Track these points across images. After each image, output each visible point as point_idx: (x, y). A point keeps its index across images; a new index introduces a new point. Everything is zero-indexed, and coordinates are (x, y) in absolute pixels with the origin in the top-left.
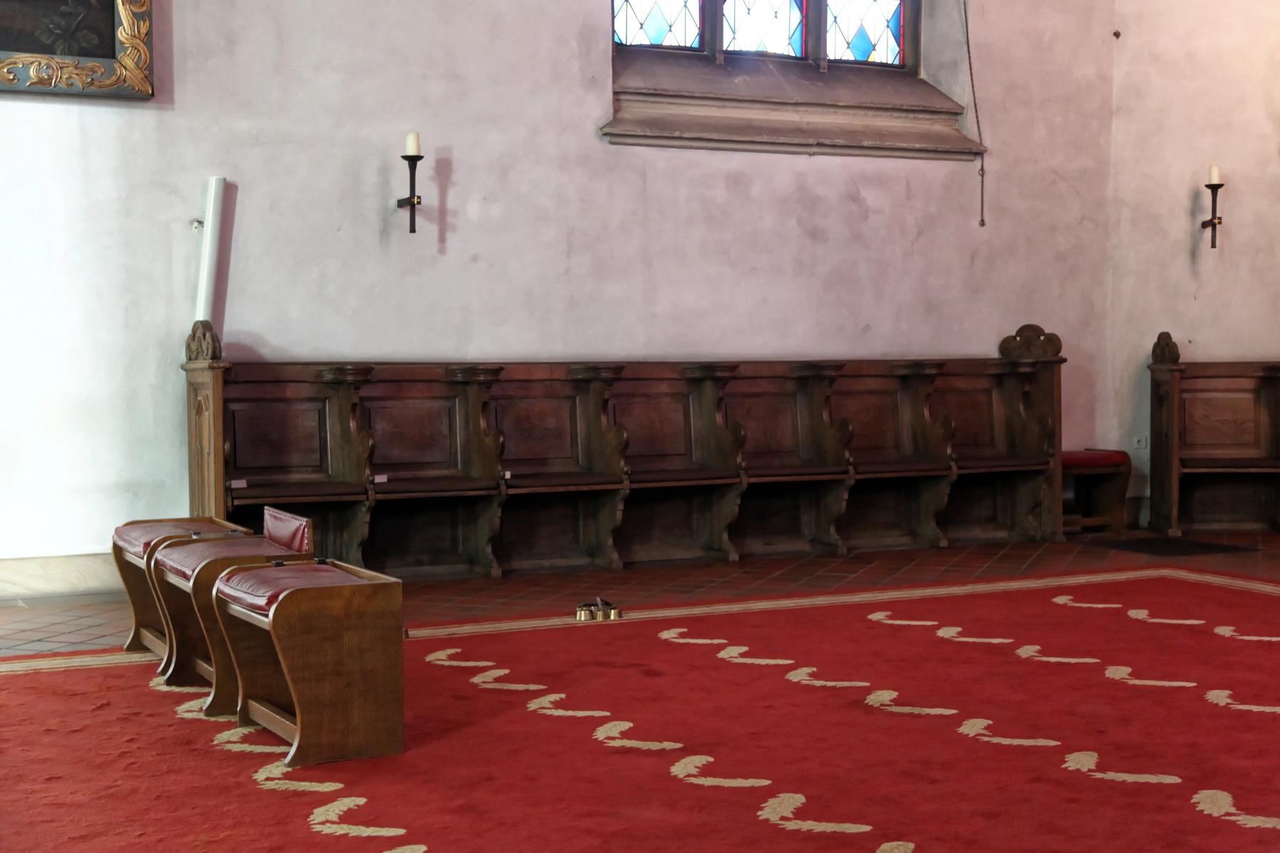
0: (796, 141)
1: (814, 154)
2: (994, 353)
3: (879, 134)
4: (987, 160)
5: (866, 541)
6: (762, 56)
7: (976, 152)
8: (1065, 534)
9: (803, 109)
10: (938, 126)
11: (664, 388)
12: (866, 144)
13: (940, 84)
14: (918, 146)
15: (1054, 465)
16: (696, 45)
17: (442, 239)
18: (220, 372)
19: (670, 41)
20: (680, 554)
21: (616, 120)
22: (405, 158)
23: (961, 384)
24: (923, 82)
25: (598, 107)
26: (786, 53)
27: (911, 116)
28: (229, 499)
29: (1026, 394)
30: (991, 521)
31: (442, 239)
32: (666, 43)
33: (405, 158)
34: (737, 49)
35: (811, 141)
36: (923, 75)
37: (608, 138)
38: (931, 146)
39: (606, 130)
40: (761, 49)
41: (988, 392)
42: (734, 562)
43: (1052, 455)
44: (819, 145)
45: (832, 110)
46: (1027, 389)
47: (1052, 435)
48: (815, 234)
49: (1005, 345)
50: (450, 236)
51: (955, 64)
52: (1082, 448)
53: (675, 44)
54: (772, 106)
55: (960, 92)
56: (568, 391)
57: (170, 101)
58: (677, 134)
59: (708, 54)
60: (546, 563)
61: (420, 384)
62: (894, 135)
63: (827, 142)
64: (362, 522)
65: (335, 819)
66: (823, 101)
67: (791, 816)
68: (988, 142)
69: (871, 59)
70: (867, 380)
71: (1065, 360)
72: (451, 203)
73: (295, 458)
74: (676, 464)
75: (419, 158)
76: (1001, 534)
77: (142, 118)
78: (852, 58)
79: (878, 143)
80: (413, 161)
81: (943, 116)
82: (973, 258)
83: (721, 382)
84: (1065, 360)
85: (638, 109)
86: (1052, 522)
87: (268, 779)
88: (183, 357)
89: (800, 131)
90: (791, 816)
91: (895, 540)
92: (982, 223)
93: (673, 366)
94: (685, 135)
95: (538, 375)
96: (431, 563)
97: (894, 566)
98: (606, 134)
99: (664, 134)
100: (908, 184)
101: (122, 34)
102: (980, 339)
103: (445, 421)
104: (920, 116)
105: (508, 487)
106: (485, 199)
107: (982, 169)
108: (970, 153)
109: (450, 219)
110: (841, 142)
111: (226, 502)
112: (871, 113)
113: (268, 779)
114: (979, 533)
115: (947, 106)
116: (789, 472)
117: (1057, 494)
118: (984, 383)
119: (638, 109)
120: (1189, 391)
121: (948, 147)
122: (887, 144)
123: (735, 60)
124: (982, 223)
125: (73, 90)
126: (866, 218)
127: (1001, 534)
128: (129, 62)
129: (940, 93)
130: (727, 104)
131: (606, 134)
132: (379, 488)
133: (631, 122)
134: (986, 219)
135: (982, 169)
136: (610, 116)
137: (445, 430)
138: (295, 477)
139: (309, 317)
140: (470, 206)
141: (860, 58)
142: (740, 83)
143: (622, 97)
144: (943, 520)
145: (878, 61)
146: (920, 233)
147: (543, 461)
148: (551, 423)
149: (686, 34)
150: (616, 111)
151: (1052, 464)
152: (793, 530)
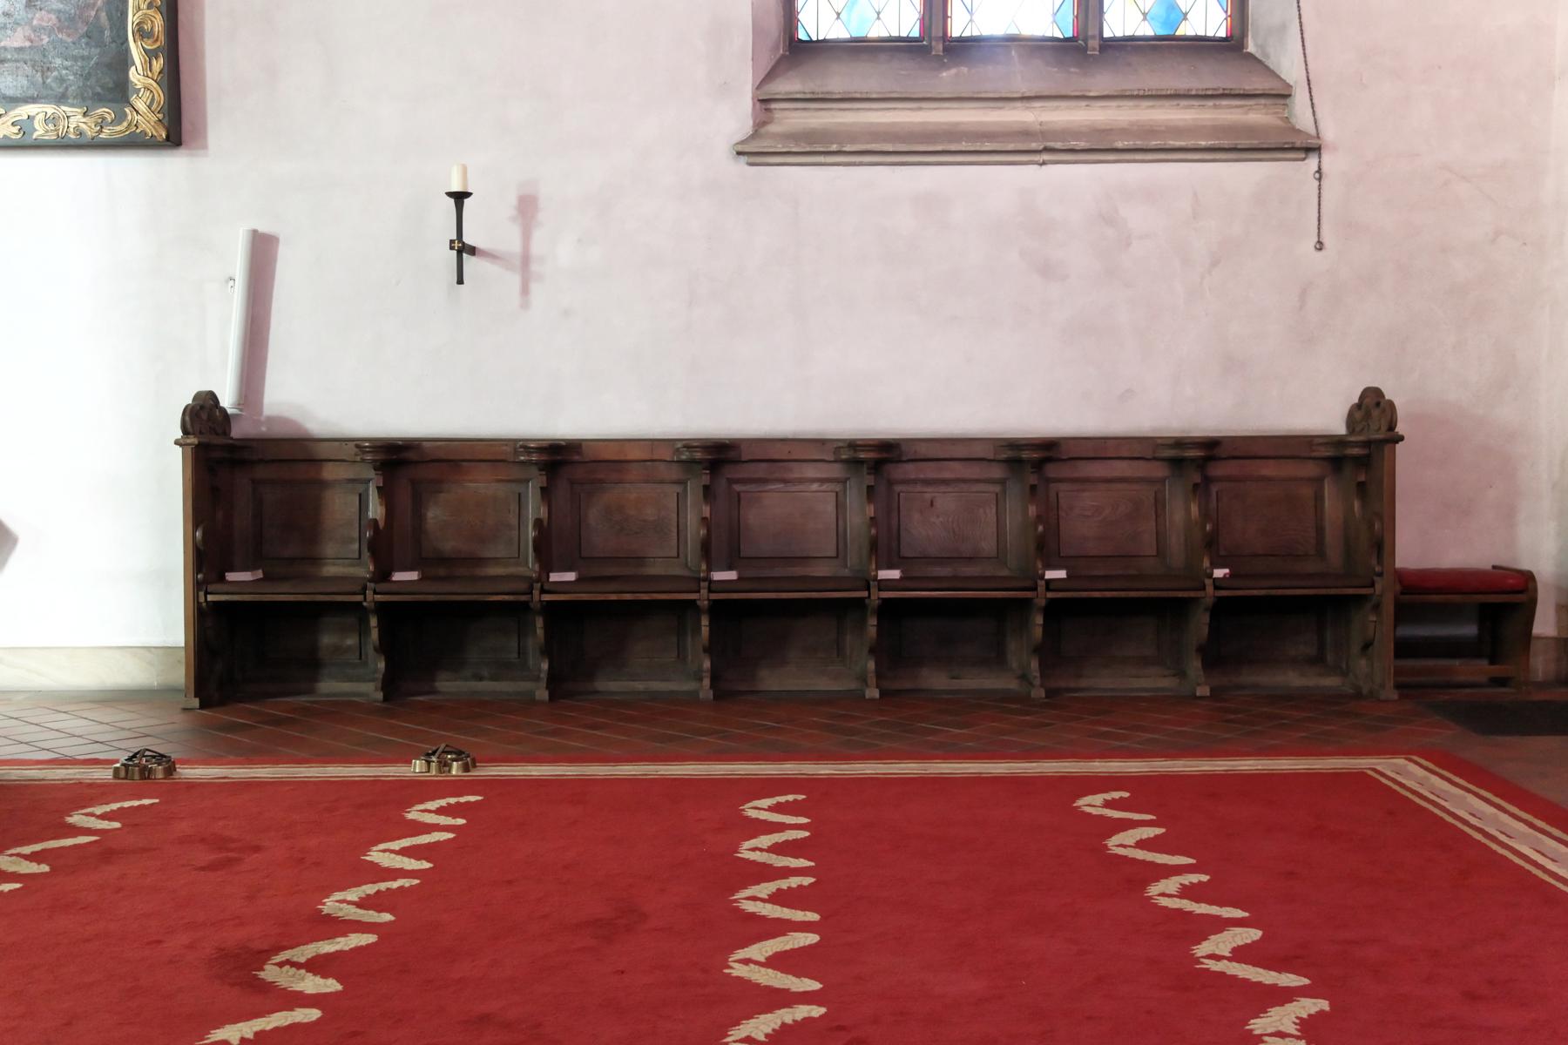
0: (1011, 147)
1: (1044, 163)
2: (1340, 428)
3: (1150, 131)
4: (1326, 157)
5: (1103, 681)
6: (1012, 41)
7: (1312, 149)
8: (1398, 686)
9: (1037, 104)
10: (1257, 116)
11: (810, 471)
12: (1119, 145)
13: (1267, 56)
14: (1203, 143)
15: (1385, 590)
16: (916, 33)
17: (525, 290)
18: (189, 449)
19: (876, 31)
20: (823, 684)
21: (755, 135)
22: (450, 194)
23: (1269, 469)
24: (1251, 56)
25: (736, 117)
26: (1049, 34)
27: (1210, 103)
28: (202, 594)
29: (1361, 485)
30: (1317, 661)
31: (525, 290)
32: (873, 34)
33: (450, 194)
34: (976, 33)
35: (1034, 146)
36: (1251, 48)
37: (744, 159)
38: (1225, 143)
39: (740, 148)
40: (1013, 31)
41: (1319, 481)
42: (872, 700)
43: (1380, 575)
44: (1047, 150)
45: (1083, 103)
46: (1362, 478)
47: (1382, 544)
48: (1048, 270)
49: (1351, 420)
50: (535, 287)
51: (1283, 28)
52: (1489, 567)
53: (885, 34)
54: (992, 104)
55: (1289, 67)
56: (675, 473)
57: (205, 147)
58: (834, 147)
59: (935, 47)
60: (640, 686)
61: (483, 465)
62: (1177, 131)
63: (1058, 145)
64: (1200, 625)
65: (762, 959)
66: (1063, 93)
67: (1292, 1029)
68: (1329, 134)
69: (1179, 32)
70: (752, 466)
71: (1402, 438)
72: (537, 248)
73: (330, 549)
74: (821, 570)
75: (468, 195)
76: (1331, 682)
77: (172, 164)
78: (1150, 32)
79: (1139, 143)
80: (460, 197)
81: (1263, 101)
82: (1303, 294)
83: (877, 467)
84: (1402, 438)
85: (793, 120)
86: (1375, 670)
87: (1163, 895)
88: (179, 434)
89: (1026, 133)
90: (1292, 1029)
91: (1154, 681)
92: (1320, 246)
93: (821, 443)
94: (847, 149)
95: (634, 454)
96: (494, 678)
97: (1115, 722)
98: (739, 153)
99: (818, 149)
100: (1195, 194)
101: (136, 76)
102: (1323, 412)
103: (514, 507)
104: (1225, 102)
105: (1048, 589)
106: (579, 240)
107: (1319, 171)
108: (1293, 149)
109: (534, 267)
110: (1082, 145)
111: (196, 597)
112: (1114, 103)
113: (1163, 895)
114: (1293, 679)
115: (1258, 84)
116: (945, 585)
117: (1379, 626)
118: (1311, 470)
119: (793, 120)
120: (738, 481)
121: (1255, 143)
122: (1154, 143)
123: (963, 49)
124: (1320, 246)
125: (83, 141)
126: (1129, 245)
127: (1331, 682)
128: (141, 105)
129: (1267, 68)
130: (924, 105)
131: (739, 153)
132: (1218, 584)
133: (775, 136)
134: (1326, 240)
135: (1319, 171)
136: (748, 128)
137: (514, 522)
138: (330, 570)
139: (344, 386)
140: (559, 248)
141: (1161, 32)
142: (990, 76)
143: (773, 106)
144: (1213, 658)
145: (1190, 33)
146: (1215, 263)
147: (640, 560)
148: (650, 513)
149: (905, 21)
150: (759, 125)
151: (1378, 587)
152: (996, 658)
